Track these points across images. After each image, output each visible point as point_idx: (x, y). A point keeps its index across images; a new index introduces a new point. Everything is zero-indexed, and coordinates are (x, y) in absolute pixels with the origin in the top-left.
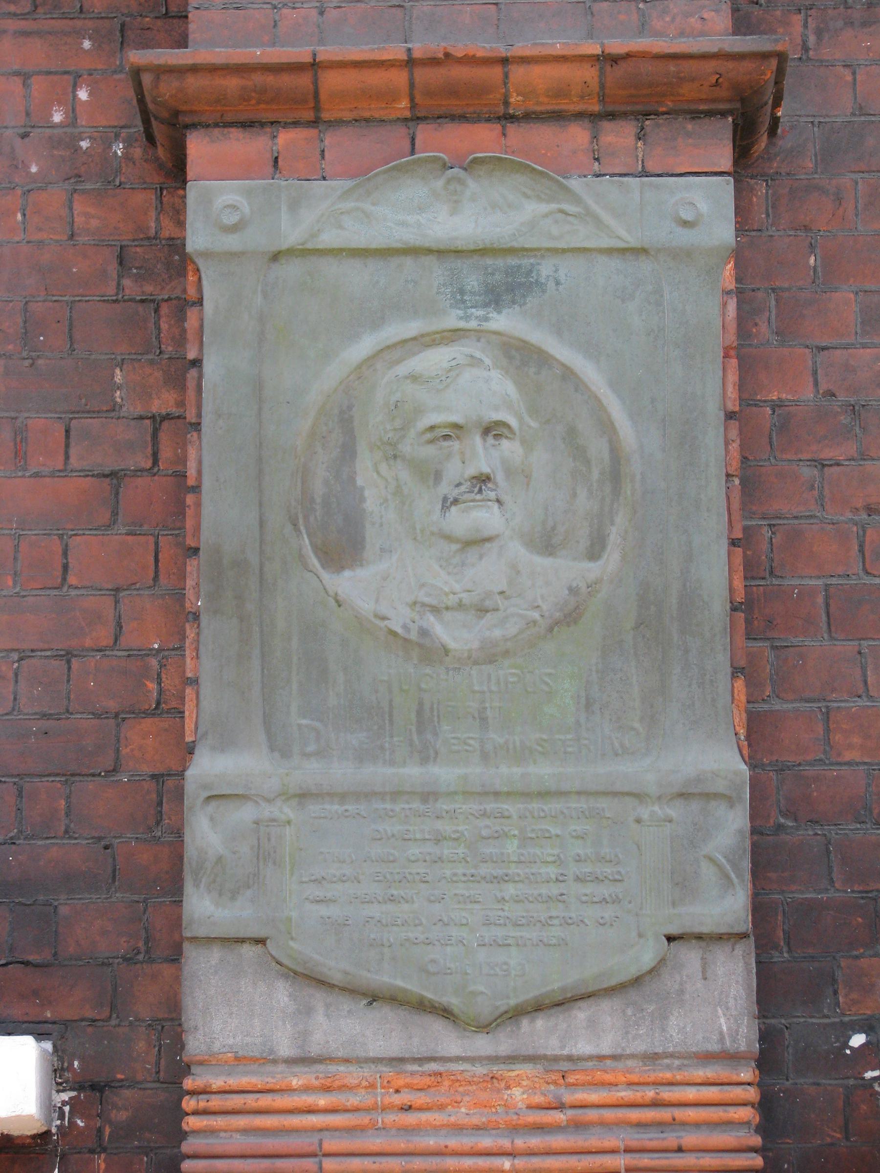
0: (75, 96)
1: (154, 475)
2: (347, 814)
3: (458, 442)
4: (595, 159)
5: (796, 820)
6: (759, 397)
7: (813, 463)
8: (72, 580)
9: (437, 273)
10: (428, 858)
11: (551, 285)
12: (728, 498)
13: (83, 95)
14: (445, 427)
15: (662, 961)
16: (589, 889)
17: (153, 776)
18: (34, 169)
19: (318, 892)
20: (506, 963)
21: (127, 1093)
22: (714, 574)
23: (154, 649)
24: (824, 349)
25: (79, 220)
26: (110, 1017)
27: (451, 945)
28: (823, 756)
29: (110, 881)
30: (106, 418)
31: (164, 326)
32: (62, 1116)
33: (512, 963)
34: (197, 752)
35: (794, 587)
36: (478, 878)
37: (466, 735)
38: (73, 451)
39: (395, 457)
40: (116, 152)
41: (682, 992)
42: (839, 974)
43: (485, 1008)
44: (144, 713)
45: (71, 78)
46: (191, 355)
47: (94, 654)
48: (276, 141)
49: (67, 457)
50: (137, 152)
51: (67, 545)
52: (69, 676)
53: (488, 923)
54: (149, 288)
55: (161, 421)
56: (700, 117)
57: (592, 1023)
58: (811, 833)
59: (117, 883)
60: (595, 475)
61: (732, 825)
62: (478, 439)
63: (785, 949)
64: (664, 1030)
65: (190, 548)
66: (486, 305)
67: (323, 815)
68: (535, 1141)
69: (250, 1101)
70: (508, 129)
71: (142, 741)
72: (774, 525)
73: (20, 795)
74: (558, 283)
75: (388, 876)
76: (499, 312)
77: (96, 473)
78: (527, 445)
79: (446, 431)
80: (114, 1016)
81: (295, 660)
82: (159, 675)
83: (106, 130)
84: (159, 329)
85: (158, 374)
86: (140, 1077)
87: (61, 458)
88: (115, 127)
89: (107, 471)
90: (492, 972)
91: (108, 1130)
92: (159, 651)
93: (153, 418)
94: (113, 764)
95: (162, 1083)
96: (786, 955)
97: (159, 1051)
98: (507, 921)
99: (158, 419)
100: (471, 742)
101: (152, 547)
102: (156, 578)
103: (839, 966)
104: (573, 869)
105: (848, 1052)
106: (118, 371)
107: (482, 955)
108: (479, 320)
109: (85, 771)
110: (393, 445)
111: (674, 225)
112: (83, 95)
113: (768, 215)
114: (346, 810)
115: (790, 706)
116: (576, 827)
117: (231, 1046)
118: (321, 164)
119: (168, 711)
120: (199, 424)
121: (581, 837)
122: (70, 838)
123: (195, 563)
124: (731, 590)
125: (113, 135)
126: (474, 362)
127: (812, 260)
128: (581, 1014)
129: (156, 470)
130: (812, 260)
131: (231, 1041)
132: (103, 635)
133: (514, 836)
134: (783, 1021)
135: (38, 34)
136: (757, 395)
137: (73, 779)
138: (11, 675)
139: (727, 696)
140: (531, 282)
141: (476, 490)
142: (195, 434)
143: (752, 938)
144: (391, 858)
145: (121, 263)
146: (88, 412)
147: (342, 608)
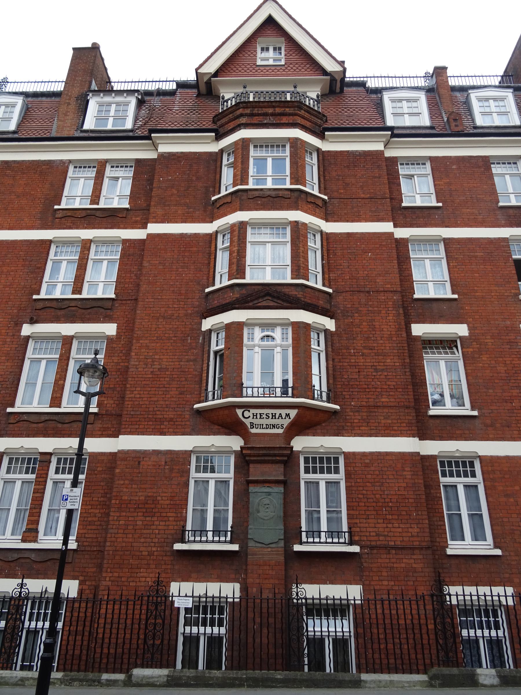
61: (283, 532)
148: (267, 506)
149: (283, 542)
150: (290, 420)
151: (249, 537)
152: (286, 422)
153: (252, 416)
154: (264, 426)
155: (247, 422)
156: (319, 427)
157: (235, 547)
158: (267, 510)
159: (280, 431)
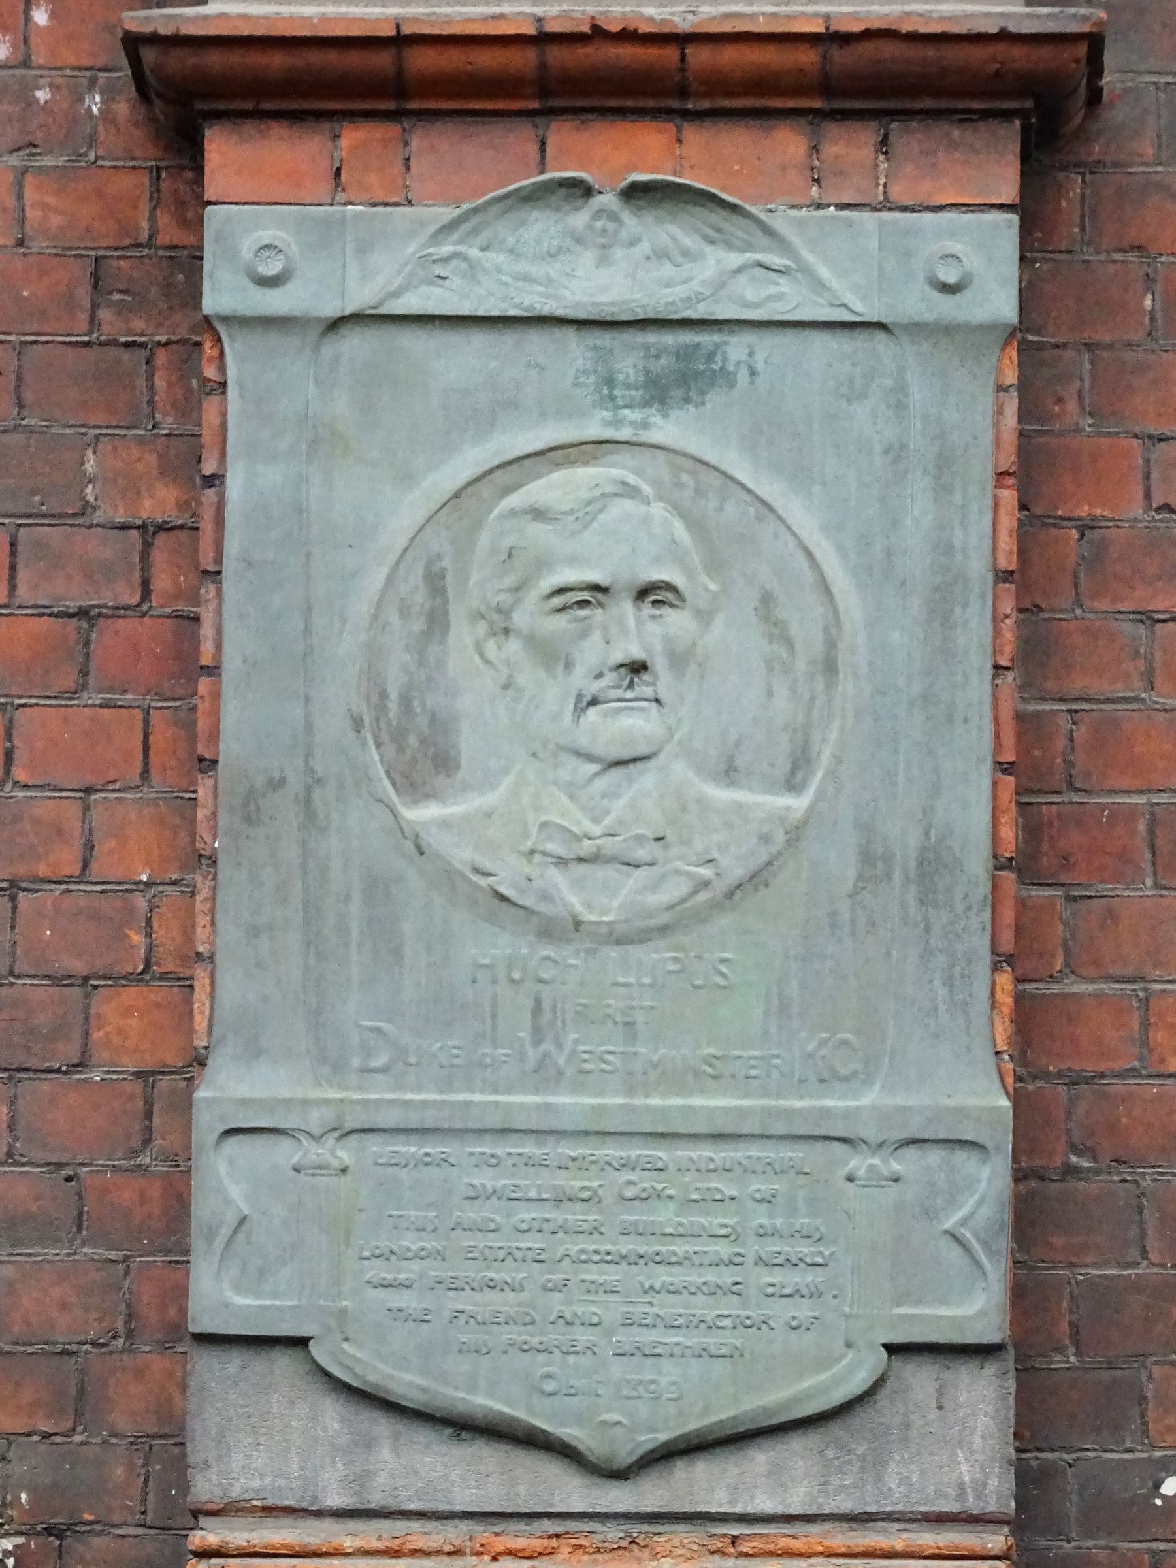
0: (28, 19)
1: (144, 615)
2: (428, 1159)
3: (600, 611)
4: (814, 180)
5: (1095, 1159)
6: (1060, 513)
7: (1138, 617)
8: (19, 774)
9: (576, 351)
10: (545, 1226)
11: (743, 376)
12: (995, 699)
13: (40, 17)
14: (581, 589)
15: (879, 1383)
16: (775, 1277)
17: (138, 1074)
19: (377, 1270)
20: (653, 1382)
21: (97, 1541)
22: (971, 812)
23: (141, 882)
26: (74, 1430)
27: (576, 1353)
28: (1136, 1064)
29: (74, 1229)
30: (71, 525)
31: (160, 383)
33: (664, 1381)
34: (209, 1062)
35: (1105, 806)
36: (617, 1258)
37: (603, 1048)
38: (22, 575)
39: (506, 631)
40: (90, 109)
41: (908, 1426)
42: (1150, 1390)
43: (625, 1456)
44: (125, 978)
46: (209, 468)
47: (52, 887)
48: (337, 143)
49: (13, 587)
50: (122, 108)
51: (11, 721)
52: (13, 919)
53: (628, 1323)
54: (138, 324)
55: (155, 533)
56: (972, 120)
57: (775, 1470)
58: (1116, 1178)
59: (84, 1233)
60: (801, 665)
63: (1072, 1350)
65: (201, 760)
66: (646, 404)
67: (393, 1161)
70: (684, 132)
71: (124, 1025)
72: (1076, 711)
74: (753, 373)
75: (487, 1252)
76: (665, 416)
77: (56, 610)
78: (705, 617)
79: (585, 595)
80: (80, 1428)
81: (355, 933)
82: (149, 921)
83: (76, 73)
84: (151, 388)
85: (152, 459)
86: (116, 1518)
88: (88, 69)
89: (72, 605)
90: (634, 1393)
92: (149, 884)
93: (143, 527)
94: (79, 1055)
95: (151, 1528)
96: (1072, 1359)
97: (146, 1481)
98: (658, 1321)
99: (151, 529)
100: (609, 1058)
102: (145, 773)
103: (1150, 1377)
104: (753, 1248)
105: (1159, 1502)
106: (90, 453)
107: (617, 1369)
108: (636, 428)
109: (34, 1063)
111: (927, 288)
112: (40, 17)
113: (1083, 229)
114: (427, 1155)
115: (1090, 988)
117: (257, 1491)
118: (405, 179)
119: (163, 976)
120: (219, 573)
121: (767, 1201)
122: (17, 1164)
123: (210, 782)
124: (995, 839)
125: (85, 82)
126: (629, 491)
127: (1148, 303)
128: (760, 1457)
129: (145, 607)
130: (1148, 303)
131: (256, 1484)
132: (67, 860)
133: (670, 1197)
134: (1065, 1456)
136: (1058, 509)
137: (19, 1075)
139: (984, 991)
140: (714, 371)
141: (626, 683)
142: (212, 588)
143: (1011, 1350)
144: (492, 1226)
145: (95, 286)
146: (44, 516)
147: (424, 857)
148: (632, 632)
149: (981, 1404)
151: (220, 1295)
158: (633, 725)
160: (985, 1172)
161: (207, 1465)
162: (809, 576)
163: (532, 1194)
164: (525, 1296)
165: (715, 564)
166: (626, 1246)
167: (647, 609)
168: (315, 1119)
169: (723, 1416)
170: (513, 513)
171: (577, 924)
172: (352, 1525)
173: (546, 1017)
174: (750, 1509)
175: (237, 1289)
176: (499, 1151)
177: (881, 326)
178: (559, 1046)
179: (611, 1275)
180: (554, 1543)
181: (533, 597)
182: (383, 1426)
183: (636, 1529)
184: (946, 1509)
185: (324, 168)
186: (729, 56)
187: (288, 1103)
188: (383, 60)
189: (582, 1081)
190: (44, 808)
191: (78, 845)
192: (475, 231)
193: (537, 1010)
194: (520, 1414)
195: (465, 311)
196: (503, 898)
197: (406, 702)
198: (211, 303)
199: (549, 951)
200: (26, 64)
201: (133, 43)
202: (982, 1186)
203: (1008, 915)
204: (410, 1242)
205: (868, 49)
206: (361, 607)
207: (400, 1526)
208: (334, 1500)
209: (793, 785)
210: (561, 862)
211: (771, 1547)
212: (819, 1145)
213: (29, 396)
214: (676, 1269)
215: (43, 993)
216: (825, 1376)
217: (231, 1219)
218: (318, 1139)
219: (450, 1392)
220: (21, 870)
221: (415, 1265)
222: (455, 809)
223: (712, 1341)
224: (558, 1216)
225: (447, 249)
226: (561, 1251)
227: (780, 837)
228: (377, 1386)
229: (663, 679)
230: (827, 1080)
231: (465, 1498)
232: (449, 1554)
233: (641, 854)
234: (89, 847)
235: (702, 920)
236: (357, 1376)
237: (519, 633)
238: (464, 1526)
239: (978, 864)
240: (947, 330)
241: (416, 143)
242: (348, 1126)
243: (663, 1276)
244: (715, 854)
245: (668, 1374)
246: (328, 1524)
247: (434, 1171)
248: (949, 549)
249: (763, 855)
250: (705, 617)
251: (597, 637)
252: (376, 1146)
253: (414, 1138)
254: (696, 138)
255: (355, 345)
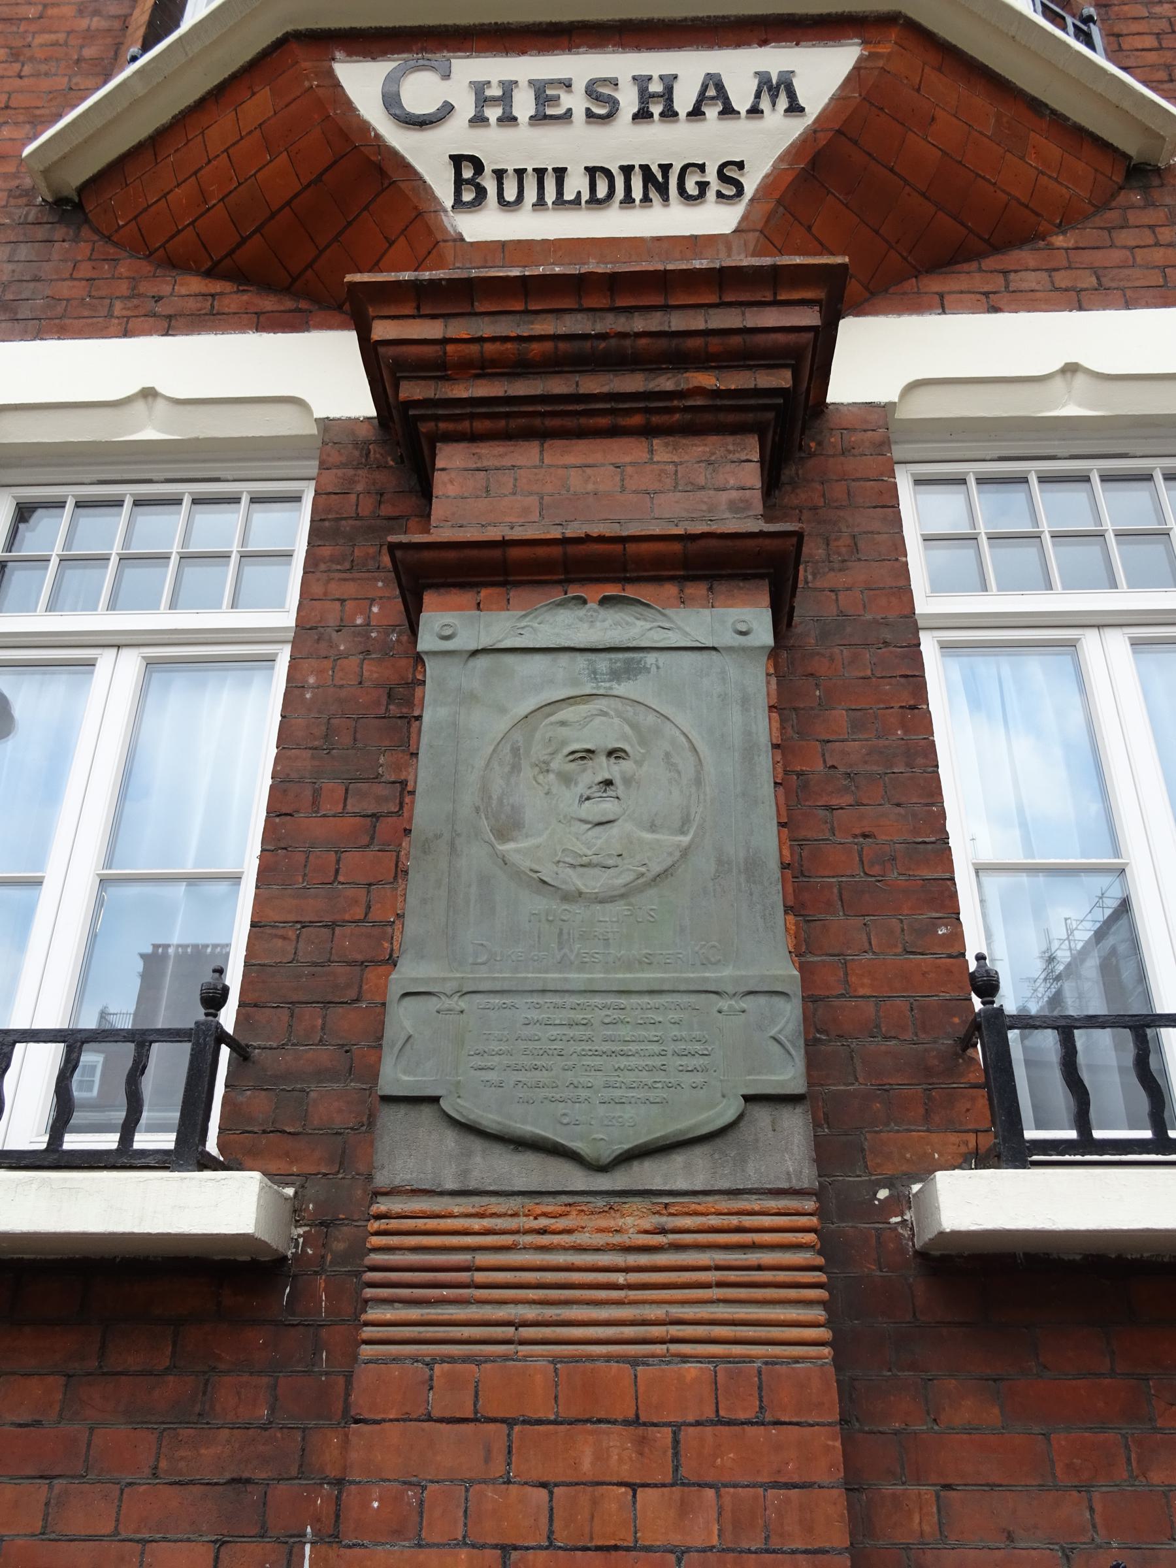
8: (341, 878)
9: (581, 661)
11: (654, 669)
15: (741, 1117)
16: (684, 1061)
18: (342, 648)
19: (479, 1061)
24: (828, 741)
25: (366, 674)
32: (296, 1247)
33: (626, 1116)
38: (349, 801)
39: (548, 771)
41: (757, 1140)
42: (866, 1145)
43: (607, 1153)
45: (368, 602)
46: (416, 714)
61: (788, 1016)
62: (603, 759)
64: (743, 1171)
66: (610, 680)
68: (644, 1259)
69: (420, 1224)
73: (292, 1016)
74: (658, 668)
78: (639, 763)
86: (356, 1218)
87: (341, 806)
89: (370, 812)
91: (329, 1257)
101: (394, 858)
104: (672, 1047)
107: (601, 1110)
110: (546, 763)
116: (673, 1016)
126: (604, 714)
127: (818, 693)
128: (678, 1159)
130: (818, 693)
132: (359, 913)
135: (353, 580)
138: (294, 937)
148: (605, 768)
149: (794, 1126)
150: (797, 127)
151: (395, 1076)
152: (763, 145)
153: (466, 107)
154: (576, 184)
155: (428, 157)
156: (1025, 256)
157: (226, 1205)
158: (607, 807)
159: (717, 219)
160: (789, 1007)
161: (383, 1167)
162: (686, 745)
163: (557, 1022)
164: (553, 1073)
165: (643, 742)
166: (606, 1047)
167: (612, 760)
168: (449, 987)
169: (658, 1135)
170: (552, 724)
171: (580, 894)
172: (459, 1200)
173: (565, 937)
174: (674, 1188)
175: (405, 1073)
176: (540, 1001)
177: (714, 649)
178: (572, 951)
179: (598, 1061)
180: (568, 1209)
181: (560, 756)
182: (477, 1144)
183: (613, 1200)
184: (781, 1186)
185: (474, 603)
186: (645, 547)
187: (435, 980)
188: (497, 553)
189: (582, 967)
190: (350, 892)
191: (364, 906)
192: (536, 617)
193: (561, 933)
194: (549, 1134)
195: (531, 646)
196: (544, 882)
197: (500, 800)
198: (422, 646)
199: (566, 907)
200: (368, 625)
201: (393, 548)
202: (788, 1014)
203: (790, 890)
204: (494, 1046)
205: (702, 543)
206: (480, 763)
207: (485, 1200)
208: (450, 1185)
209: (683, 833)
210: (572, 866)
211: (686, 1210)
212: (703, 996)
213: (358, 736)
214: (631, 1058)
215: (340, 969)
216: (711, 1113)
217: (403, 1037)
218: (450, 996)
219: (512, 1124)
220: (337, 917)
221: (496, 1058)
222: (523, 844)
223: (652, 1095)
224: (571, 1033)
225: (523, 624)
226: (572, 1050)
227: (677, 854)
228: (475, 1122)
229: (620, 789)
230: (706, 964)
231: (520, 1184)
232: (511, 1215)
233: (610, 862)
234: (369, 907)
235: (642, 891)
236: (464, 1116)
237: (553, 771)
238: (519, 1199)
239: (774, 865)
240: (744, 649)
241: (511, 594)
242: (465, 990)
243: (624, 1062)
244: (646, 861)
245: (628, 1113)
246: (446, 1200)
247: (507, 1012)
248: (750, 734)
249: (669, 862)
250: (639, 763)
251: (589, 771)
252: (478, 999)
253: (498, 996)
254: (628, 587)
255: (482, 662)
